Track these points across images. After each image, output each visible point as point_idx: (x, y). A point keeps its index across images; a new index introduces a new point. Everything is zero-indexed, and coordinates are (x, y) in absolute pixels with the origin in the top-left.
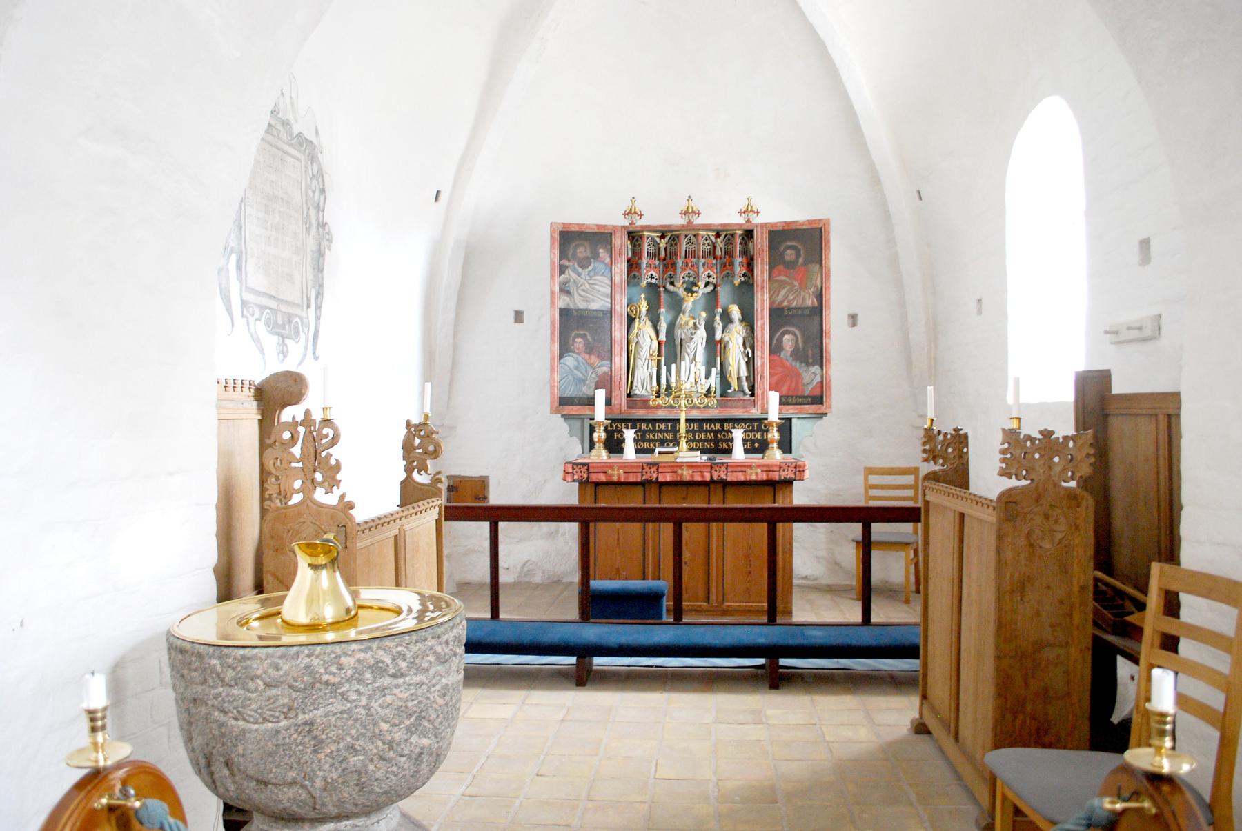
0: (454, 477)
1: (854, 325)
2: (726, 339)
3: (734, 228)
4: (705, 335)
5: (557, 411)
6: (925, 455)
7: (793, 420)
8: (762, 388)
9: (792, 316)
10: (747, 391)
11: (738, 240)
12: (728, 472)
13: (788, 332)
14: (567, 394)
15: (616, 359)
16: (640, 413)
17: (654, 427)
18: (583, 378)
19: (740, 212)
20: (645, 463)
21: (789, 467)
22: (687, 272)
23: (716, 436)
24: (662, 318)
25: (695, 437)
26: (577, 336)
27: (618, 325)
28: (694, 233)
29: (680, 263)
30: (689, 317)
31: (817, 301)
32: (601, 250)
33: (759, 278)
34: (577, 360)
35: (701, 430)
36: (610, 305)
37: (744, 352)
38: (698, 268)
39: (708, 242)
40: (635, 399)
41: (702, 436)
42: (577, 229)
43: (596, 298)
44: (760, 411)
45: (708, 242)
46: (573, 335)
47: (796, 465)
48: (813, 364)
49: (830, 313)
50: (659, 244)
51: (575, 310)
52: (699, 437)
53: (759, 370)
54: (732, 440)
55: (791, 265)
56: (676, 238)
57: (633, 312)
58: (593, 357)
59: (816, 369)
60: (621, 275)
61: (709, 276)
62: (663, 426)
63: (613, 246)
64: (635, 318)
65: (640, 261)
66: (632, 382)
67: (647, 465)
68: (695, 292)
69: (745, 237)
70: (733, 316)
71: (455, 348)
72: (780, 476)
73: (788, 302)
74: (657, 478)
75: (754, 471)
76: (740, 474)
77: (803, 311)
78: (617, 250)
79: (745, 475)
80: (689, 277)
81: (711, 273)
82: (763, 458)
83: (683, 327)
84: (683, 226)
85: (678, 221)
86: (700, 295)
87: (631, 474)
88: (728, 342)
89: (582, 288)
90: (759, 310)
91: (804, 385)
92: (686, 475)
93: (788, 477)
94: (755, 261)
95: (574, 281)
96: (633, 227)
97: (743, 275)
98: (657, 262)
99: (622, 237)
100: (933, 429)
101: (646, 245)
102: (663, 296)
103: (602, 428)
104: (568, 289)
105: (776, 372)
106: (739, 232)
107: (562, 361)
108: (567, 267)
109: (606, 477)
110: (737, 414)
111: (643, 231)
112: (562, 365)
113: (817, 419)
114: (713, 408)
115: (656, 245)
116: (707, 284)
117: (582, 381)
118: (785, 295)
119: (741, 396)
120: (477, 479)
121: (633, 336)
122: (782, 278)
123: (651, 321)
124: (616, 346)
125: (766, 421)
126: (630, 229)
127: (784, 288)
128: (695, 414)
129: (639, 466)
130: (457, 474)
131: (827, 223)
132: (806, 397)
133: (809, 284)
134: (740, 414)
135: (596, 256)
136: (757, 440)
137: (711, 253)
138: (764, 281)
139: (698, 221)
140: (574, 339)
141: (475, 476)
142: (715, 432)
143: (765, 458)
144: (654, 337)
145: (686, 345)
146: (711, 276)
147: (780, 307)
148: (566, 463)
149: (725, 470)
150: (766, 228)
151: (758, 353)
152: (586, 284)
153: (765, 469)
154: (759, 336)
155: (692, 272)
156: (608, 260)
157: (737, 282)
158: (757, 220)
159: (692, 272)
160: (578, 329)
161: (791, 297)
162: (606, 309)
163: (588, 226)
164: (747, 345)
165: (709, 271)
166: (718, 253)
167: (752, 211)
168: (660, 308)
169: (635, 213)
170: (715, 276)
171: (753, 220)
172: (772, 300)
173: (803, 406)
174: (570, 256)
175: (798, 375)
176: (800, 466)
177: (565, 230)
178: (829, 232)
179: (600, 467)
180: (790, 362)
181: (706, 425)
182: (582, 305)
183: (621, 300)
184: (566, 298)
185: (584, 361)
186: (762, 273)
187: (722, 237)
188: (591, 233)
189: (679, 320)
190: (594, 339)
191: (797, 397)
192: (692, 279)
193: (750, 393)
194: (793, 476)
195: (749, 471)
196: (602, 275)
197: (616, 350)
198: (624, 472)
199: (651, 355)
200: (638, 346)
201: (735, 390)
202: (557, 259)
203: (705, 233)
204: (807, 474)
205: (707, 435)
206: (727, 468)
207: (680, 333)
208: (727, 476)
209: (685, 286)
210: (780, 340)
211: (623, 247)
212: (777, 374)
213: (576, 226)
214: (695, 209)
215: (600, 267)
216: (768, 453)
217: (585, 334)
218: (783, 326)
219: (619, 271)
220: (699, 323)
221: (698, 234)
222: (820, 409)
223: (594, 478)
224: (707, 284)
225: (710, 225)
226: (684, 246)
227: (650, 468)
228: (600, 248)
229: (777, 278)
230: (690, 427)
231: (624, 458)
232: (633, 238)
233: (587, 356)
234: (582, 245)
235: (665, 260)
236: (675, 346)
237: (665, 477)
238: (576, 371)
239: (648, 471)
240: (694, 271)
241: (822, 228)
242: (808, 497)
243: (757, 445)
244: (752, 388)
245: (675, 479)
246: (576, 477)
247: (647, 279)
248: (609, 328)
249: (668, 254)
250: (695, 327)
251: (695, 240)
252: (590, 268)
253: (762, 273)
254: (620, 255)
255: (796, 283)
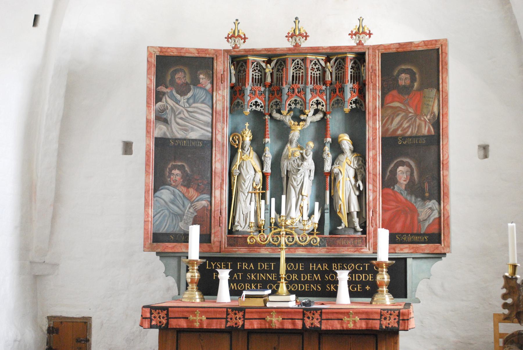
0: (55, 317)
1: (486, 156)
2: (336, 170)
3: (343, 51)
4: (313, 167)
5: (151, 249)
6: (506, 311)
7: (408, 260)
8: (374, 225)
9: (407, 145)
10: (358, 228)
11: (349, 65)
12: (322, 319)
13: (402, 164)
14: (163, 230)
15: (217, 193)
16: (241, 252)
17: (256, 266)
18: (180, 212)
19: (351, 34)
20: (230, 308)
21: (391, 314)
22: (293, 99)
23: (323, 277)
24: (267, 148)
25: (300, 279)
26: (175, 167)
27: (219, 156)
28: (302, 57)
29: (286, 89)
30: (297, 146)
31: (434, 128)
32: (201, 76)
33: (371, 104)
34: (174, 194)
35: (306, 271)
36: (210, 134)
37: (355, 185)
38: (305, 94)
39: (317, 66)
40: (236, 236)
41: (308, 277)
42: (175, 53)
43: (195, 127)
44: (372, 251)
45: (317, 66)
46: (170, 166)
47: (399, 312)
48: (430, 199)
49: (448, 141)
50: (265, 69)
51: (173, 139)
52: (304, 278)
53: (371, 204)
54: (336, 282)
55: (406, 90)
56: (283, 63)
57: (235, 142)
58: (191, 190)
59: (432, 204)
60: (224, 102)
61: (318, 103)
62: (265, 266)
63: (215, 71)
64: (238, 148)
65: (243, 87)
66: (234, 218)
67: (232, 311)
68: (304, 120)
69: (357, 60)
70: (343, 146)
71: (59, 180)
72: (381, 325)
73: (401, 131)
74: (243, 325)
75: (351, 319)
76: (336, 322)
77: (418, 141)
78: (219, 76)
79: (341, 324)
80: (296, 104)
81: (320, 100)
82: (371, 303)
83: (290, 158)
84: (290, 49)
85: (285, 44)
86: (308, 123)
87: (215, 321)
88: (338, 174)
89: (180, 116)
90: (371, 139)
91: (419, 221)
92: (276, 321)
93: (390, 326)
94: (367, 86)
95: (172, 108)
96: (236, 52)
97: (354, 102)
98: (262, 89)
99: (224, 62)
100: (516, 279)
101: (251, 70)
102: (269, 125)
103: (196, 268)
104: (165, 117)
105: (390, 207)
106: (351, 56)
107: (157, 194)
108: (164, 94)
109: (187, 323)
110: (346, 253)
111: (247, 56)
112: (158, 199)
113: (436, 259)
114: (317, 246)
115: (262, 70)
116: (316, 112)
117: (179, 216)
118: (399, 123)
119: (352, 234)
120: (79, 321)
121: (235, 168)
122: (396, 104)
123: (256, 151)
124: (217, 178)
125: (374, 262)
126: (233, 53)
127: (398, 115)
128: (301, 253)
129: (224, 312)
130: (59, 314)
131: (444, 44)
132: (424, 234)
133: (425, 111)
134: (352, 253)
135: (196, 82)
136: (368, 283)
137: (321, 79)
138: (376, 108)
139: (305, 44)
140: (171, 170)
141: (78, 316)
142: (323, 273)
143: (373, 303)
144: (258, 168)
145: (292, 177)
146: (320, 103)
147: (394, 136)
148: (144, 307)
149: (319, 317)
150: (379, 50)
151: (369, 186)
152: (185, 112)
153: (364, 316)
154: (371, 168)
155: (298, 99)
156: (209, 86)
157: (347, 108)
158: (369, 42)
159: (298, 99)
160: (175, 160)
161: (405, 125)
162: (207, 139)
163: (187, 50)
164: (359, 177)
165: (318, 98)
166: (328, 78)
167: (364, 33)
168: (265, 138)
169: (239, 36)
170: (324, 104)
171: (365, 42)
172: (385, 128)
173: (418, 245)
174: (168, 82)
175: (414, 211)
176: (404, 314)
177: (162, 54)
178: (446, 54)
179: (181, 312)
180: (405, 196)
181: (313, 265)
182: (180, 134)
183: (223, 129)
184: (162, 126)
185: (181, 195)
186: (374, 99)
187: (332, 61)
188: (192, 57)
189: (285, 150)
190: (192, 171)
191: (412, 234)
192: (298, 106)
193: (362, 230)
194: (396, 325)
195: (346, 319)
196: (202, 102)
197: (217, 182)
198: (207, 318)
199: (254, 189)
200: (241, 178)
201: (346, 227)
202: (153, 86)
203: (314, 57)
204: (412, 323)
205: (313, 276)
206: (321, 315)
207: (286, 164)
208: (321, 325)
209: (292, 113)
210: (394, 172)
211: (226, 73)
212: (392, 209)
213: (175, 51)
214: (302, 31)
215: (200, 93)
216: (377, 297)
217: (183, 166)
218: (396, 157)
219: (221, 98)
220: (306, 154)
221: (306, 58)
222: (437, 248)
223: (174, 324)
224: (316, 112)
225: (318, 48)
226: (291, 71)
227: (235, 314)
228: (201, 74)
229: (391, 105)
230: (295, 267)
231: (218, 301)
232: (238, 63)
233: (184, 189)
234: (181, 70)
235: (271, 85)
236: (281, 179)
237: (252, 324)
238: (171, 205)
239: (234, 316)
240: (301, 98)
241: (438, 49)
242: (436, 345)
243: (368, 288)
244: (364, 226)
245: (263, 327)
246: (154, 323)
247: (251, 106)
248: (210, 158)
249: (275, 80)
250: (303, 159)
251: (302, 64)
252: (189, 95)
253: (374, 99)
254: (222, 81)
255: (411, 110)
